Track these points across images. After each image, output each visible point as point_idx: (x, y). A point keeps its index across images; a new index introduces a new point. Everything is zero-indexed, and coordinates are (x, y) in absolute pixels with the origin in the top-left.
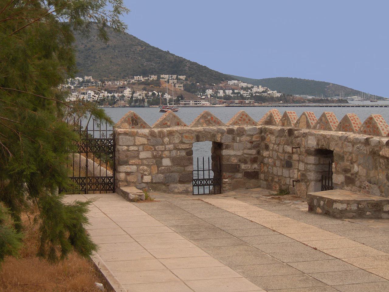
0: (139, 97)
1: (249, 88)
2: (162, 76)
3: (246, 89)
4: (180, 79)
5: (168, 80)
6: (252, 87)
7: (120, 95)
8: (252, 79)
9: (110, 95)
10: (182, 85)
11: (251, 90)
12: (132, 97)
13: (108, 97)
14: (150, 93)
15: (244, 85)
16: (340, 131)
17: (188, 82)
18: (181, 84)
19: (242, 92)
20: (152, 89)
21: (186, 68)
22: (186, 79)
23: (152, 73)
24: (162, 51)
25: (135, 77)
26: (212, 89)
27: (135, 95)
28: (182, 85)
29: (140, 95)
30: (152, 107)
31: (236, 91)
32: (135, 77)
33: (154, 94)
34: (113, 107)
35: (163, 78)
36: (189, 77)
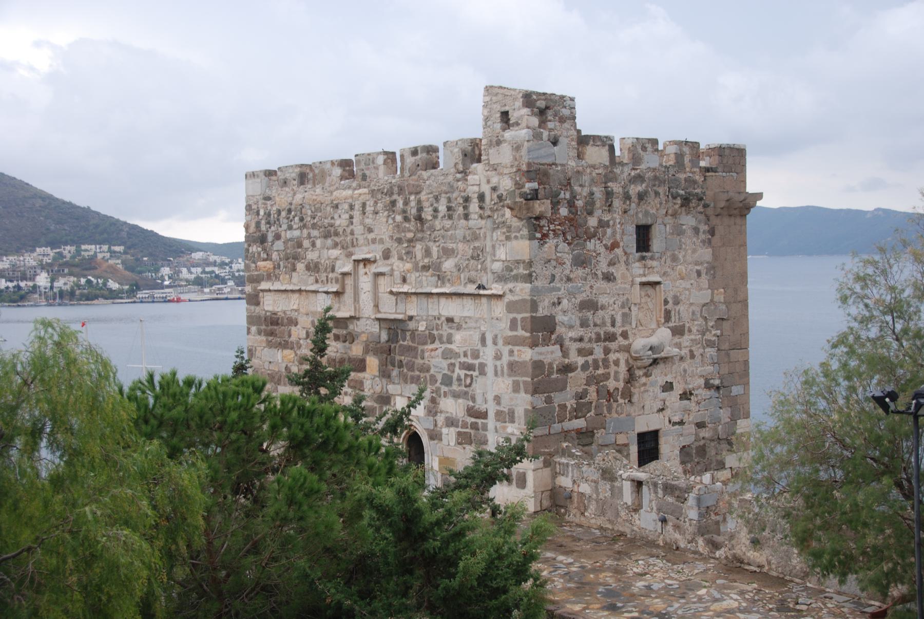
0: (64, 288)
1: (226, 264)
2: (83, 247)
3: (222, 265)
4: (115, 252)
5: (95, 253)
6: (231, 262)
7: (31, 284)
8: (15, 178)
9: (11, 285)
10: (119, 261)
11: (231, 267)
12: (52, 288)
13: (7, 288)
14: (83, 281)
15: (218, 259)
16: (440, 463)
17: (129, 256)
18: (118, 259)
19: (217, 270)
20: (86, 272)
21: (124, 234)
22: (125, 253)
23: (66, 244)
24: (79, 207)
25: (38, 249)
26: (168, 266)
27: (56, 284)
28: (119, 261)
29: (65, 284)
30: (24, 306)
31: (207, 269)
32: (38, 249)
33: (89, 282)
34: (19, 306)
35: (86, 250)
36: (129, 248)
